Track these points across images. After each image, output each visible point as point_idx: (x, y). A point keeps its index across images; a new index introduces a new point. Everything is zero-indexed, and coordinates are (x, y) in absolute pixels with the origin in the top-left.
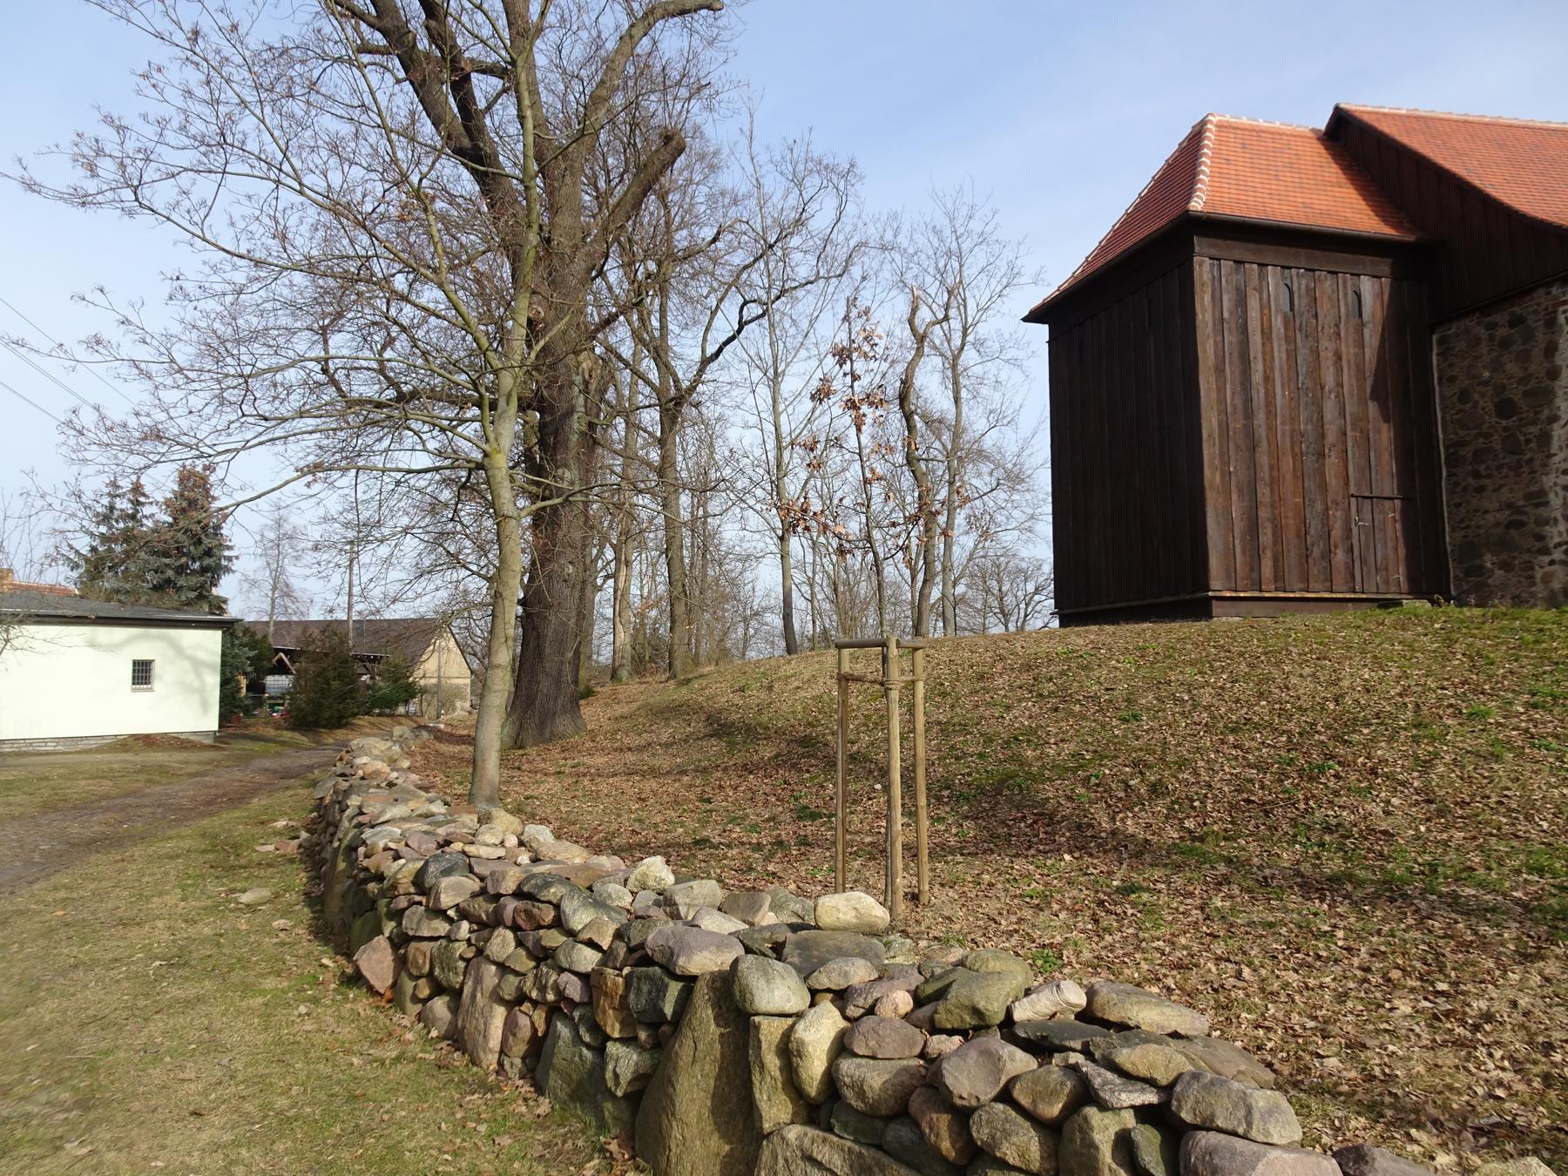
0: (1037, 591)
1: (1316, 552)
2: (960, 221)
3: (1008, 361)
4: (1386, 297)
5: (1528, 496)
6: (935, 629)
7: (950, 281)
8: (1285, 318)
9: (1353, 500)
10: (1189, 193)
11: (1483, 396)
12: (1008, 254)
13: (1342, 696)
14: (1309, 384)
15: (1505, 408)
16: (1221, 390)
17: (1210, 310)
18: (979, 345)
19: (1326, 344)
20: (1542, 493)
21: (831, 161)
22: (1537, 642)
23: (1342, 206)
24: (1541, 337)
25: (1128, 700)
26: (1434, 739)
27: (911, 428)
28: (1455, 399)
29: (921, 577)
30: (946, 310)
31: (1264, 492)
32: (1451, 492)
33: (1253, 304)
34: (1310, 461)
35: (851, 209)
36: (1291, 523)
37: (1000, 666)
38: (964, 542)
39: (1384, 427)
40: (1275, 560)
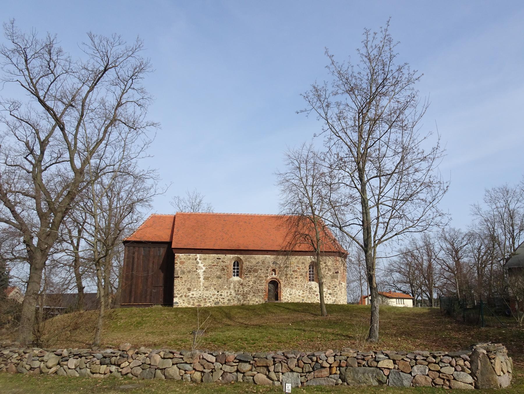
40: (135, 298)
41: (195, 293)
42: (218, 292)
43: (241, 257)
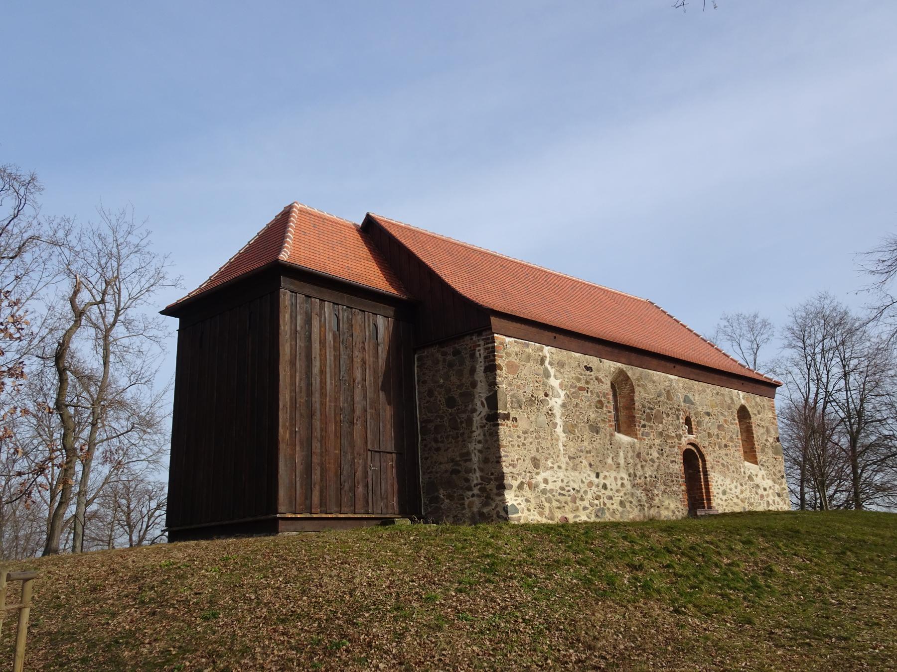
0: (158, 507)
1: (346, 487)
2: (122, 234)
3: (149, 338)
4: (391, 329)
5: (462, 455)
6: (64, 541)
7: (109, 274)
8: (334, 335)
9: (369, 453)
10: (279, 249)
11: (440, 394)
12: (156, 263)
13: (354, 590)
14: (346, 377)
15: (451, 402)
16: (293, 377)
17: (288, 324)
18: (127, 324)
19: (357, 353)
20: (468, 453)
21: (14, 171)
22: (463, 548)
23: (367, 272)
24: (468, 363)
25: (211, 602)
26: (406, 618)
27: (62, 380)
28: (426, 394)
29: (58, 498)
30: (104, 295)
31: (316, 446)
32: (423, 450)
33: (316, 323)
34: (345, 426)
35: (28, 210)
36: (332, 467)
37: (112, 578)
38: (100, 471)
39: (388, 408)
40: (321, 492)
41: (552, 477)
42: (598, 476)
43: (633, 372)
